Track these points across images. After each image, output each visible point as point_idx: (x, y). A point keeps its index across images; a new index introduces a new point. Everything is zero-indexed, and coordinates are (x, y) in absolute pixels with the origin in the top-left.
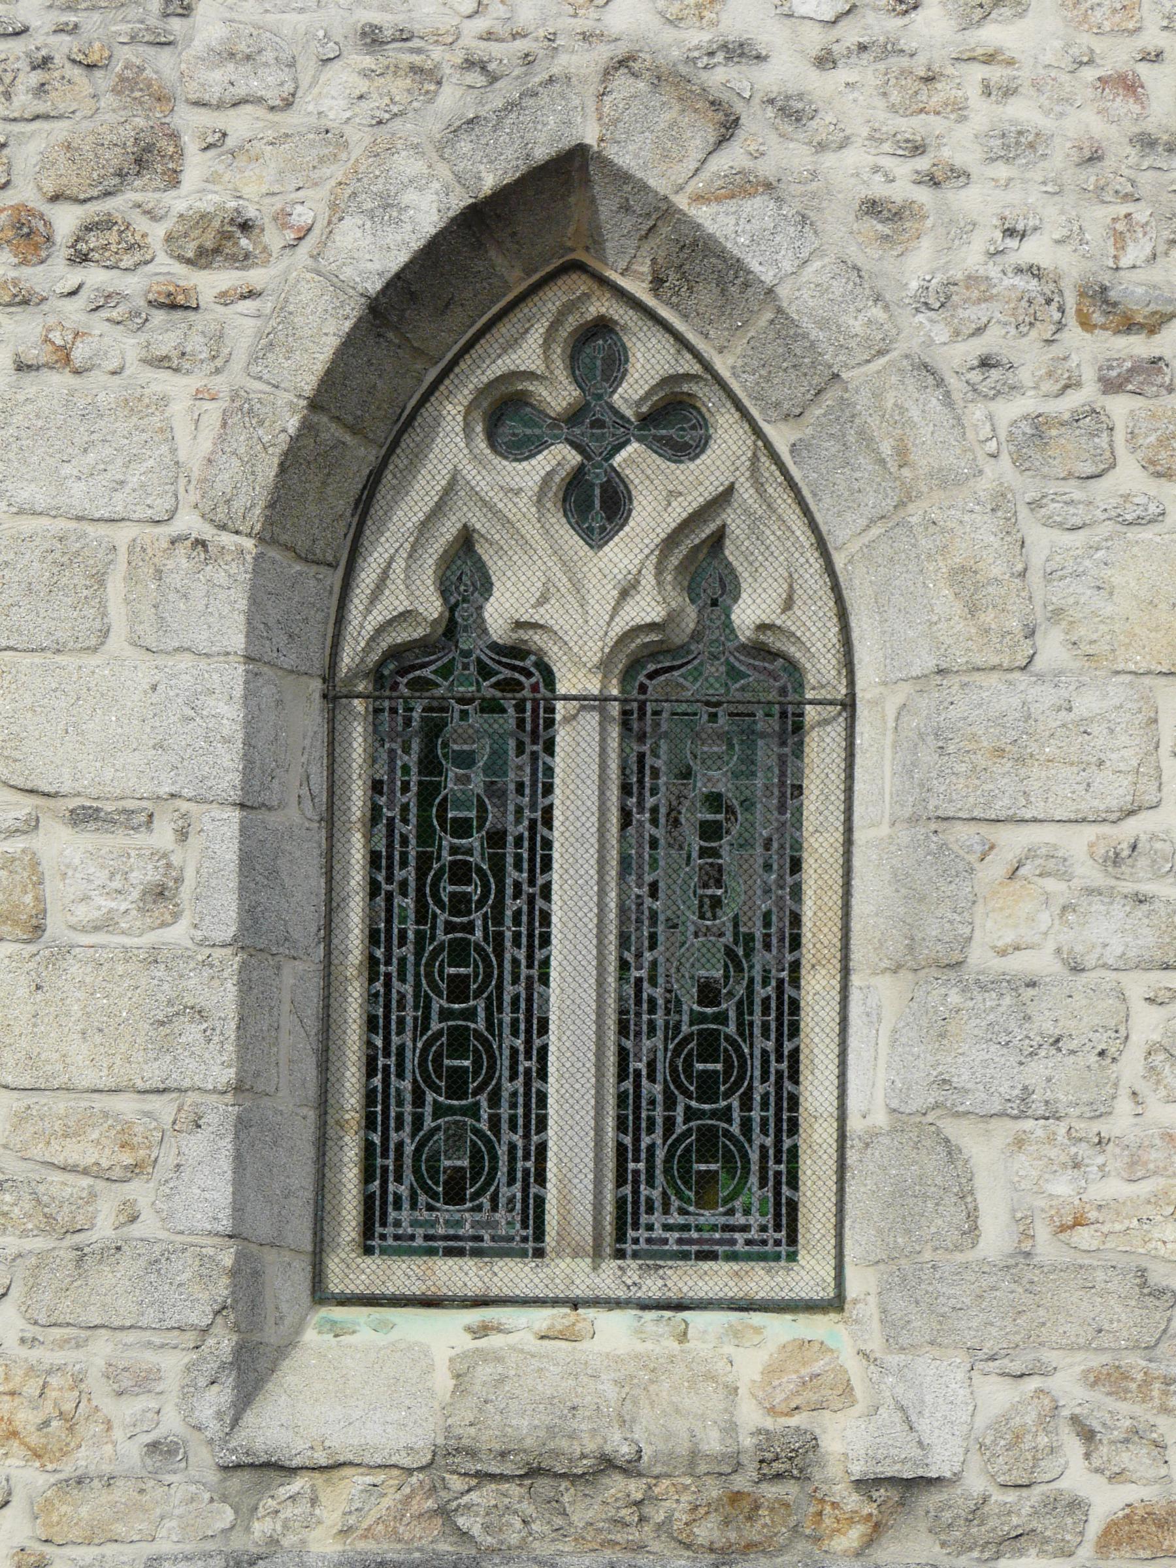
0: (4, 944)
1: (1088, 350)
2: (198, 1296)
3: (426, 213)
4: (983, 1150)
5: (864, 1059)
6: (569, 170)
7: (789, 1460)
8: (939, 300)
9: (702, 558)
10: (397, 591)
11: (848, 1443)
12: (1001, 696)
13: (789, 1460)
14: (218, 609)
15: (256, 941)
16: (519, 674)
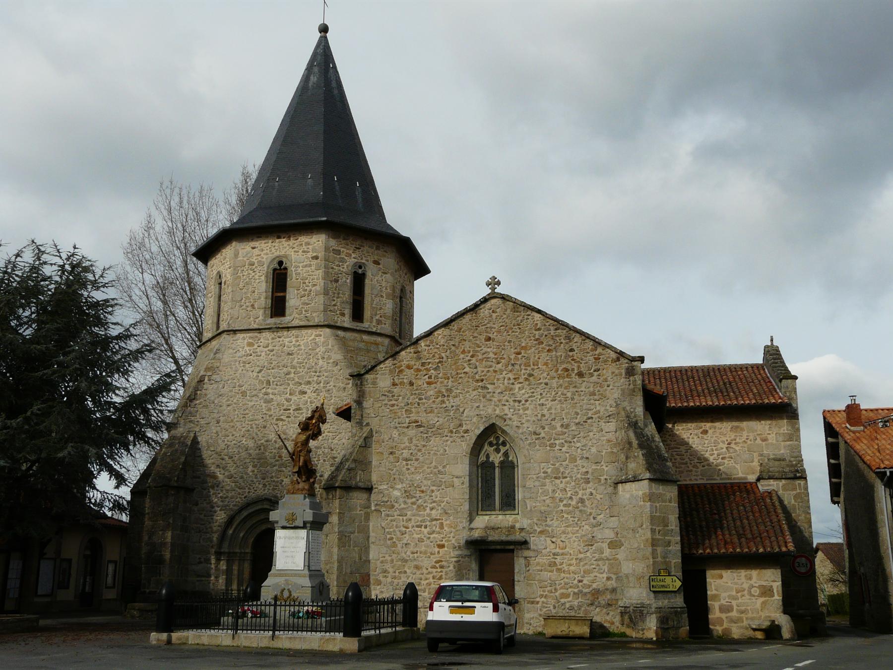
0: (887, 463)
1: (534, 437)
2: (466, 515)
3: (482, 429)
4: (528, 501)
5: (520, 495)
6: (493, 424)
7: (513, 527)
8: (522, 434)
9: (506, 454)
10: (482, 458)
11: (518, 526)
12: (527, 465)
13: (513, 527)
14: (467, 461)
15: (471, 486)
16: (493, 463)
